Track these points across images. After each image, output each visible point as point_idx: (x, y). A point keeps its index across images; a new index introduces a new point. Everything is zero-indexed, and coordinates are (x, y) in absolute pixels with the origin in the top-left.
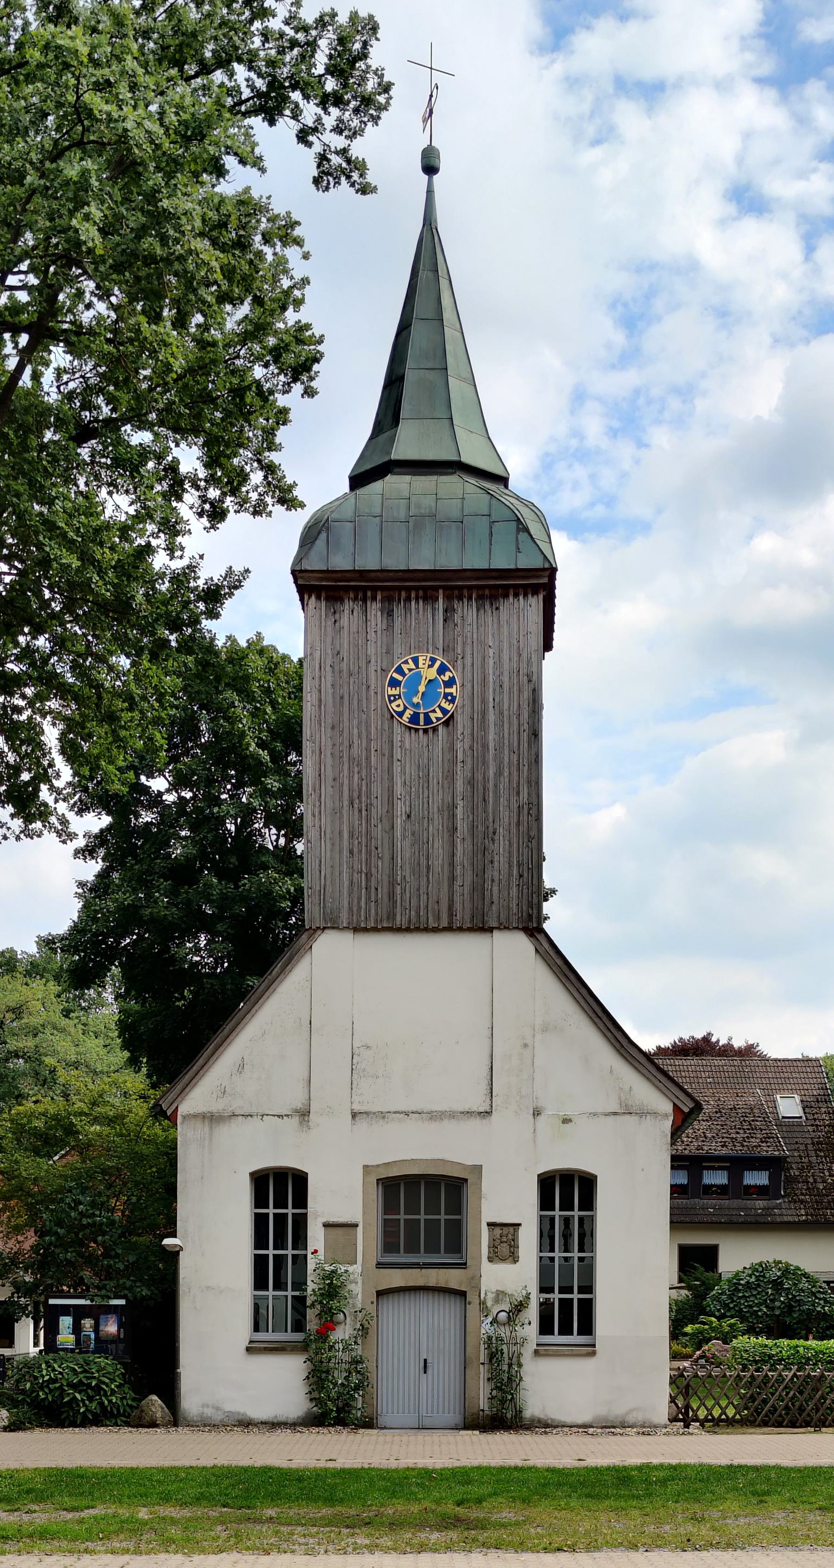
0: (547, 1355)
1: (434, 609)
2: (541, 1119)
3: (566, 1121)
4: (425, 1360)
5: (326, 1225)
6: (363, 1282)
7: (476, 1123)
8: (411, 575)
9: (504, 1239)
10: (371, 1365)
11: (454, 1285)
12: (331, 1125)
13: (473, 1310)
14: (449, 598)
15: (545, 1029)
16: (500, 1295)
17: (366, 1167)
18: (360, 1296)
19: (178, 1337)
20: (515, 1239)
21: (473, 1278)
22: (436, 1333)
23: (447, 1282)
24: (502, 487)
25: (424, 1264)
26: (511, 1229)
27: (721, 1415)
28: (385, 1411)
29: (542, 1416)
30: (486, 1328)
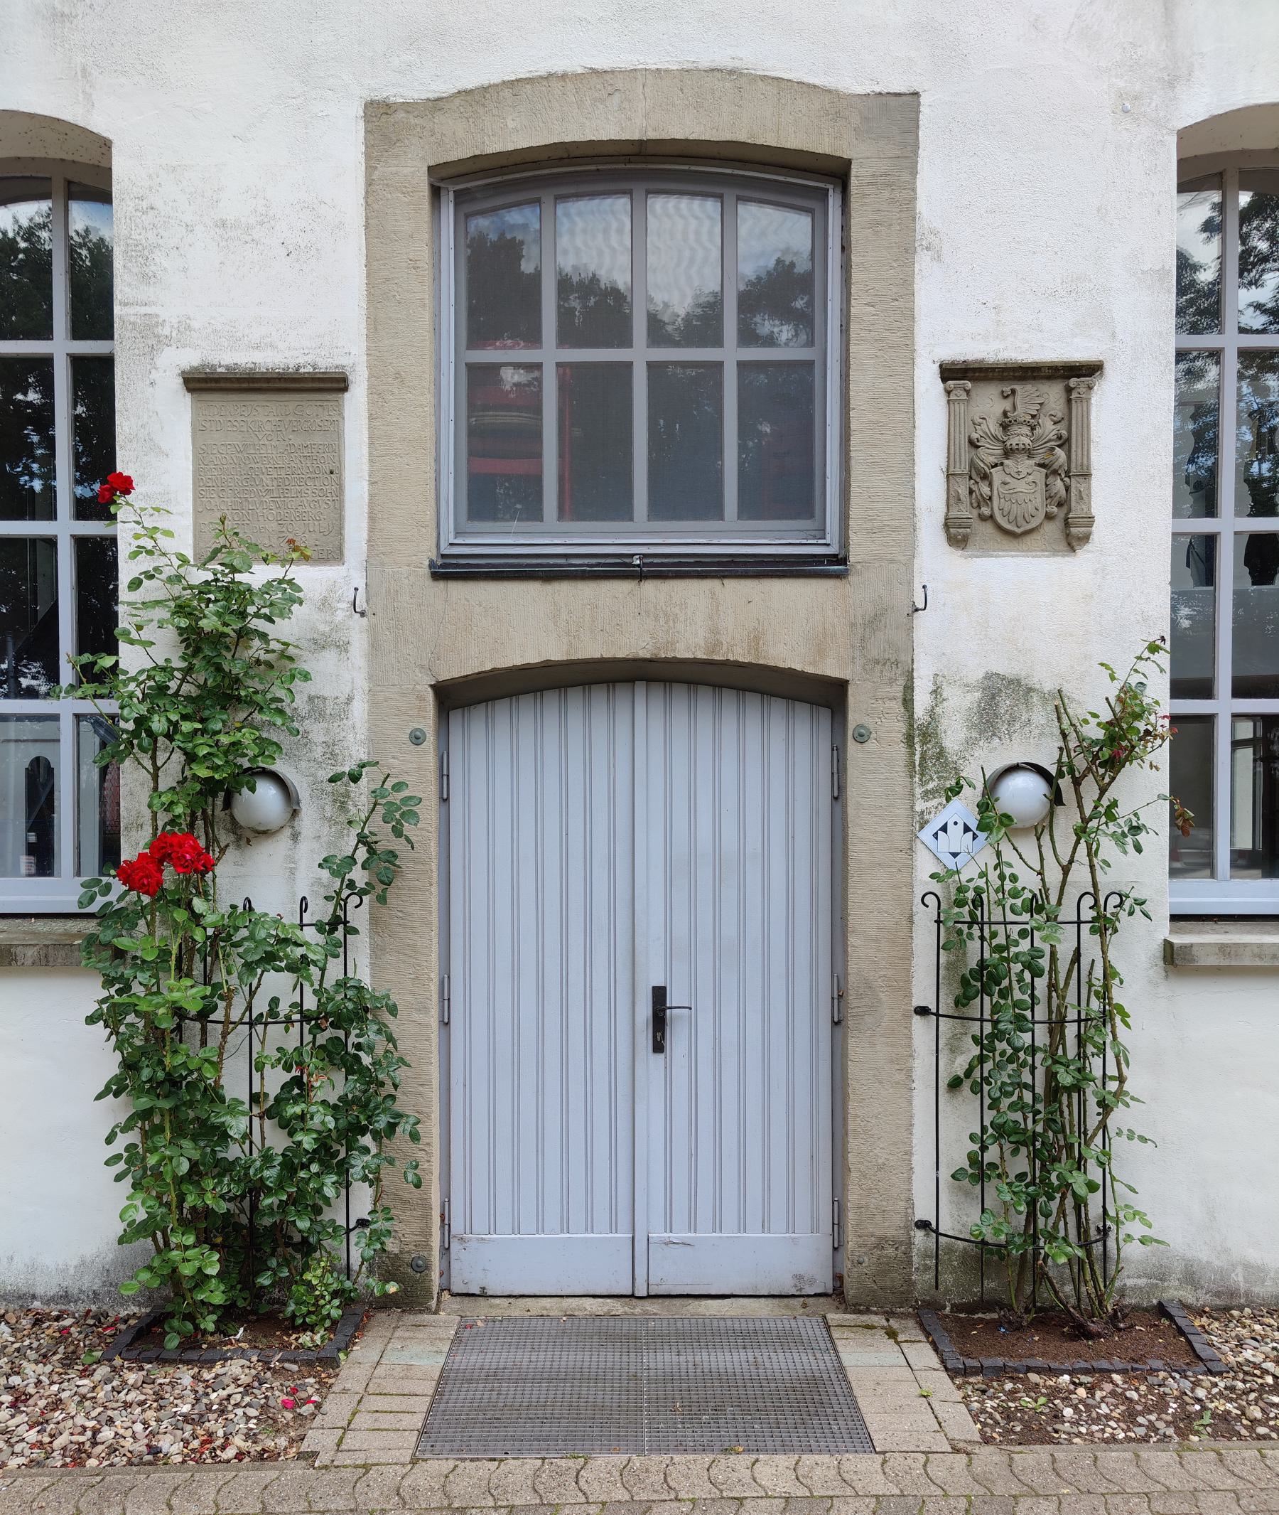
0: (1229, 969)
4: (659, 994)
5: (201, 383)
6: (374, 646)
9: (1020, 437)
10: (413, 1027)
11: (788, 653)
13: (876, 766)
16: (999, 699)
18: (359, 709)
19: (631, 335)
20: (1069, 438)
21: (874, 622)
22: (705, 874)
23: (756, 639)
26: (1052, 394)
28: (480, 1223)
29: (1203, 1254)
30: (947, 845)
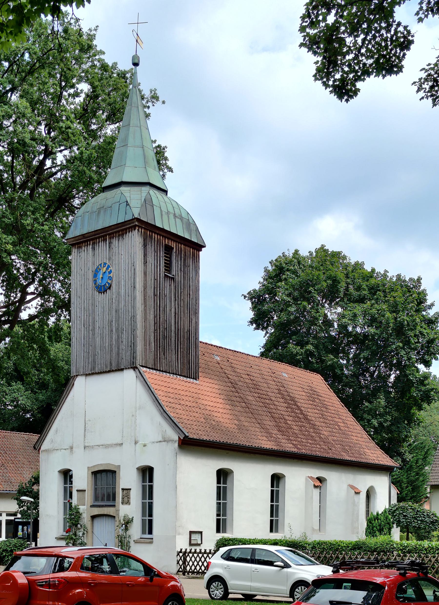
1: (106, 244)
2: (137, 445)
3: (145, 446)
5: (77, 491)
7: (118, 448)
8: (96, 233)
12: (79, 451)
14: (110, 238)
15: (140, 408)
17: (88, 467)
24: (164, 195)
25: (105, 505)
27: (194, 570)
